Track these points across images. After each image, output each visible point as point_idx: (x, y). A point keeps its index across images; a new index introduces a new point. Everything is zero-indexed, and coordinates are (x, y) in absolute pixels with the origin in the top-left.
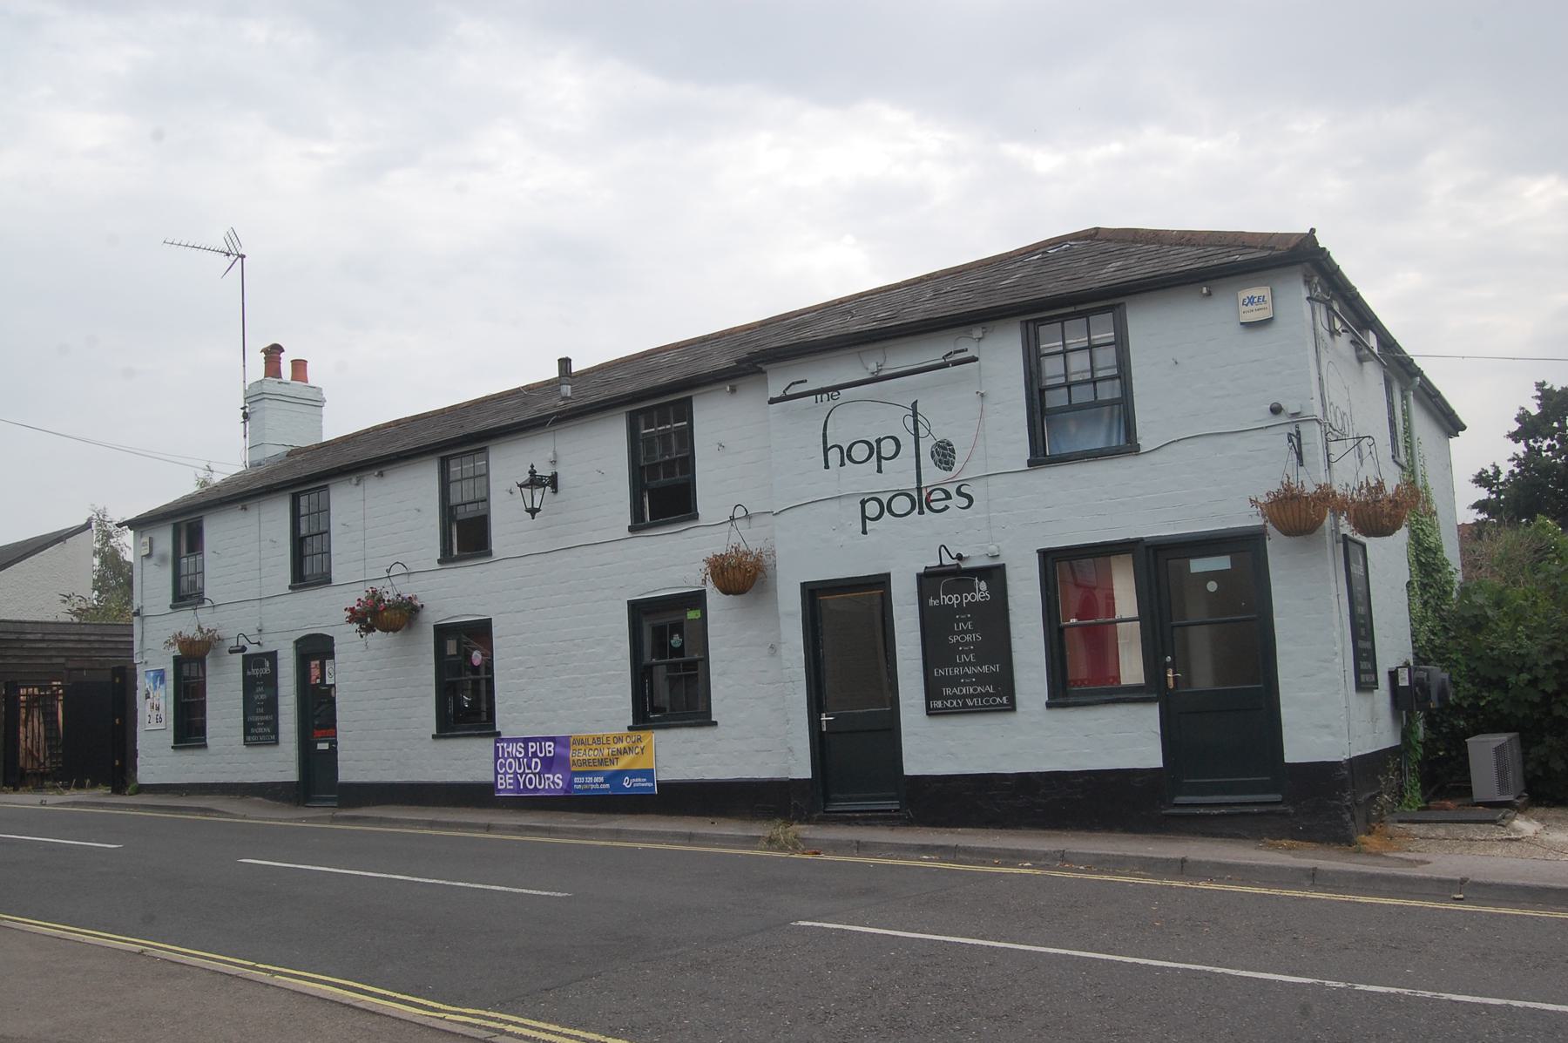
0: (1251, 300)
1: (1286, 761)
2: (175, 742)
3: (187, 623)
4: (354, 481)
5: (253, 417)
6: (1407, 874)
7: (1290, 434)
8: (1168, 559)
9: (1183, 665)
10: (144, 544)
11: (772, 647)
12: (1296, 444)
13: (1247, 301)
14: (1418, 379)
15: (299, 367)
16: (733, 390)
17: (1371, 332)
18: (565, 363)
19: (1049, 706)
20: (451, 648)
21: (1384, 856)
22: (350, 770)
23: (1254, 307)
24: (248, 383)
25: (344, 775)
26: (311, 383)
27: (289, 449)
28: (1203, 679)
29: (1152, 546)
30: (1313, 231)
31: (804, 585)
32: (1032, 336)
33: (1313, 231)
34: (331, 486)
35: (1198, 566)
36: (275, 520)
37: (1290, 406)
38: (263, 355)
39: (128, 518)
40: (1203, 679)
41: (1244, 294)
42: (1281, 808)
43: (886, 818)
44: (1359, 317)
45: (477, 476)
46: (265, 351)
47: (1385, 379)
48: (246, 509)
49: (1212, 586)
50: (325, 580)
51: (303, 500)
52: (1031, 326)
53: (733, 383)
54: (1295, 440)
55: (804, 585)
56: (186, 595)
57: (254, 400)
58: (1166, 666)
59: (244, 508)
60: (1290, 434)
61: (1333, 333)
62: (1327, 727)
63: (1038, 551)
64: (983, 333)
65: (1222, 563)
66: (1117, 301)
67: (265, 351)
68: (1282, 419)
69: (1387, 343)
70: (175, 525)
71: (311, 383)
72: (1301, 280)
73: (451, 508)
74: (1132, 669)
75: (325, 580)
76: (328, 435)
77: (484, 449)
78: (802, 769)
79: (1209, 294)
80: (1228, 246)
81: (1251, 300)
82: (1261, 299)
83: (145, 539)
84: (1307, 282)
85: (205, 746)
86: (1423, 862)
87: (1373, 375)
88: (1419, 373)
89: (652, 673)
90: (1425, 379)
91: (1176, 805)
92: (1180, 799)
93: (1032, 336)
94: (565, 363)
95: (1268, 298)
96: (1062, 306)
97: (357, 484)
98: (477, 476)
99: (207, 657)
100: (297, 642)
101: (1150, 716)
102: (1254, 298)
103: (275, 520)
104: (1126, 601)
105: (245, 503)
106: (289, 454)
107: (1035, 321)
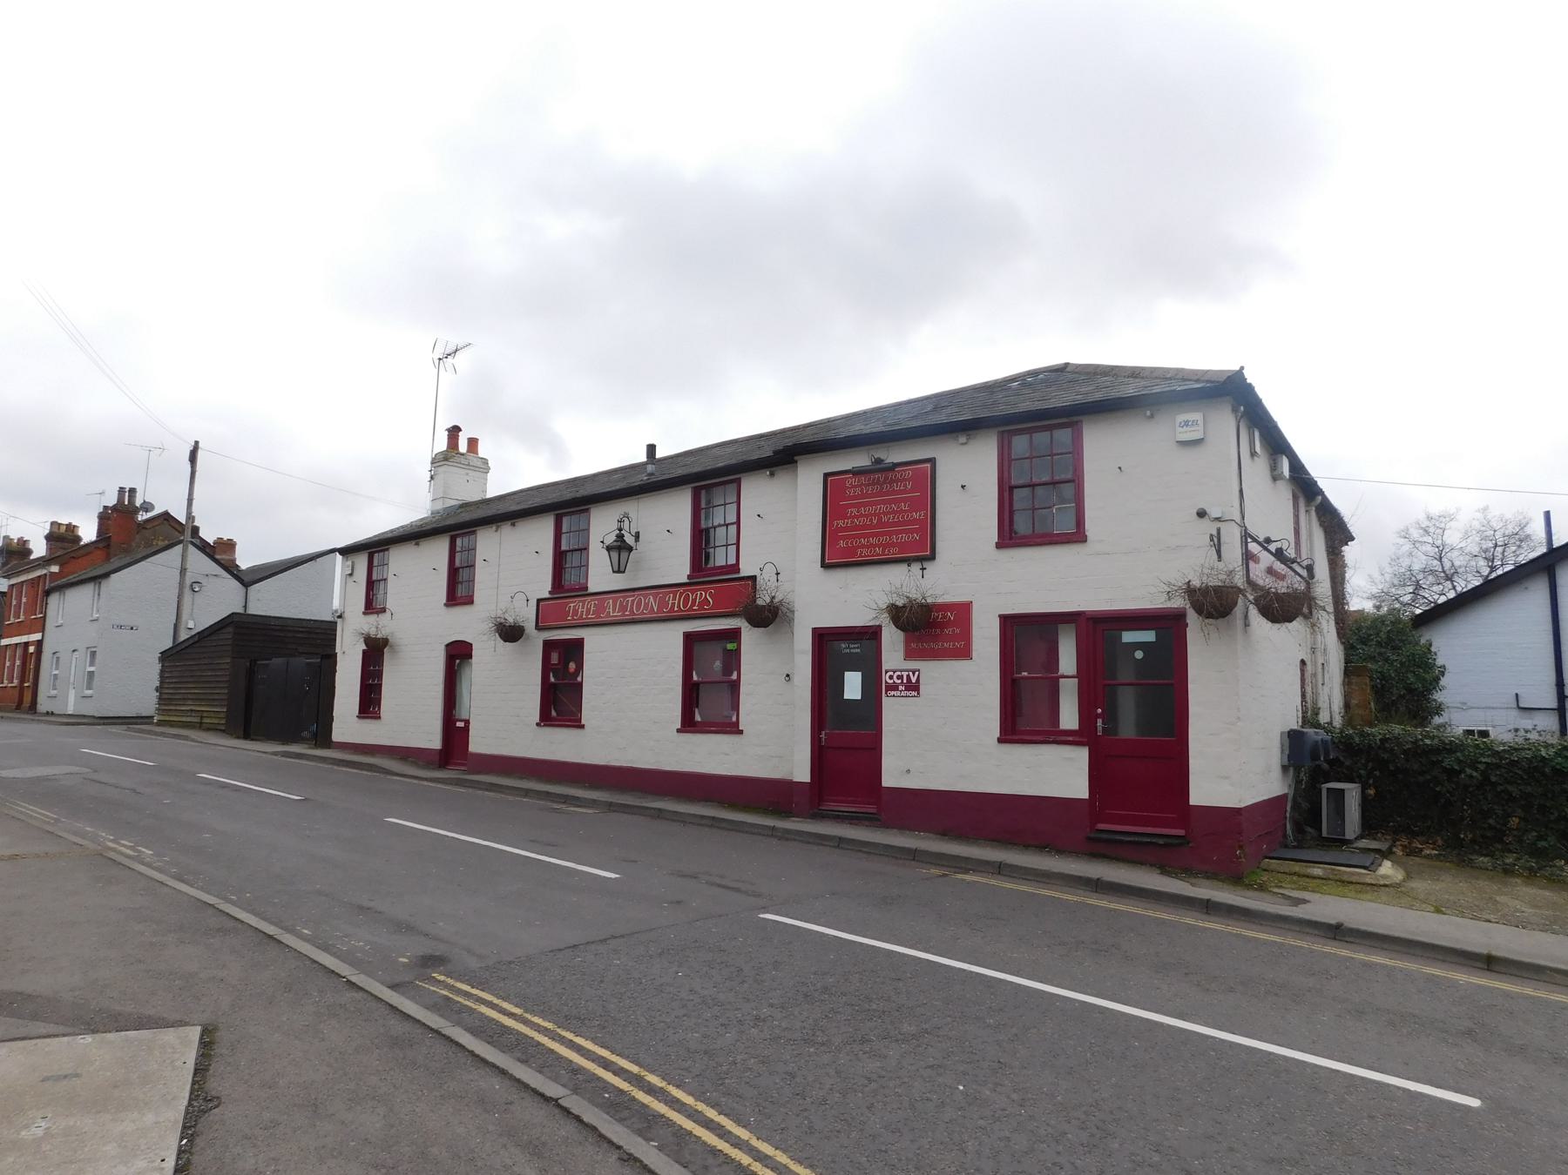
0: (1186, 423)
1: (1191, 803)
2: (360, 712)
3: (370, 624)
4: (494, 528)
5: (436, 477)
6: (1290, 914)
7: (1211, 535)
8: (1103, 630)
9: (1111, 717)
10: (348, 567)
11: (788, 676)
12: (1216, 543)
13: (1183, 424)
14: (1320, 497)
15: (473, 443)
16: (772, 474)
17: (1284, 457)
18: (651, 449)
19: (1000, 741)
20: (555, 658)
21: (1271, 891)
22: (478, 744)
23: (1189, 429)
24: (435, 452)
25: (893, 775)
26: (481, 455)
27: (461, 502)
28: (1128, 729)
29: (1092, 618)
30: (1242, 368)
31: (814, 630)
32: (1006, 442)
33: (1242, 368)
34: (592, 510)
35: (1128, 637)
36: (436, 554)
37: (1214, 512)
38: (447, 433)
39: (339, 547)
40: (1128, 729)
41: (1182, 418)
42: (876, 816)
43: (866, 819)
44: (1276, 445)
45: (1034, 457)
46: (448, 430)
47: (1293, 496)
48: (514, 525)
49: (1139, 655)
50: (469, 601)
51: (459, 542)
52: (1006, 435)
53: (772, 469)
54: (1215, 540)
55: (814, 630)
56: (372, 606)
57: (440, 460)
58: (1098, 716)
59: (513, 525)
60: (1211, 535)
61: (1253, 454)
62: (1227, 778)
63: (1000, 616)
64: (967, 439)
65: (1149, 636)
66: (1075, 419)
67: (448, 430)
68: (1205, 521)
69: (1297, 468)
70: (557, 515)
71: (481, 455)
72: (1230, 408)
73: (701, 531)
74: (1069, 718)
75: (469, 601)
76: (492, 492)
77: (587, 510)
78: (802, 772)
79: (1152, 416)
80: (1170, 379)
81: (1186, 423)
82: (1195, 423)
83: (349, 563)
84: (1235, 410)
85: (380, 717)
86: (1305, 901)
87: (1284, 493)
88: (1321, 492)
89: (698, 689)
90: (1325, 499)
91: (1097, 830)
92: (1101, 826)
93: (1006, 442)
94: (651, 449)
95: (1201, 422)
96: (1061, 417)
97: (496, 531)
98: (582, 530)
99: (385, 650)
100: (447, 645)
101: (1080, 757)
102: (1189, 422)
103: (436, 554)
104: (1068, 661)
105: (774, 469)
106: (462, 506)
107: (1009, 431)
